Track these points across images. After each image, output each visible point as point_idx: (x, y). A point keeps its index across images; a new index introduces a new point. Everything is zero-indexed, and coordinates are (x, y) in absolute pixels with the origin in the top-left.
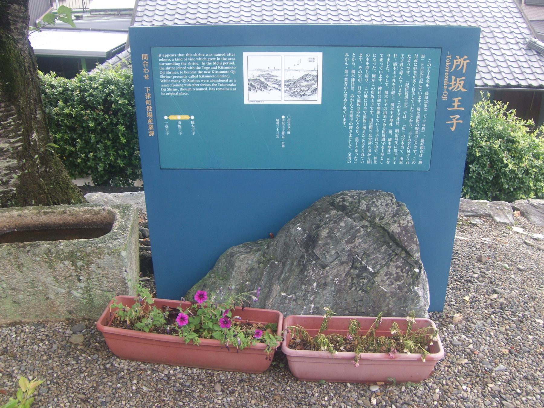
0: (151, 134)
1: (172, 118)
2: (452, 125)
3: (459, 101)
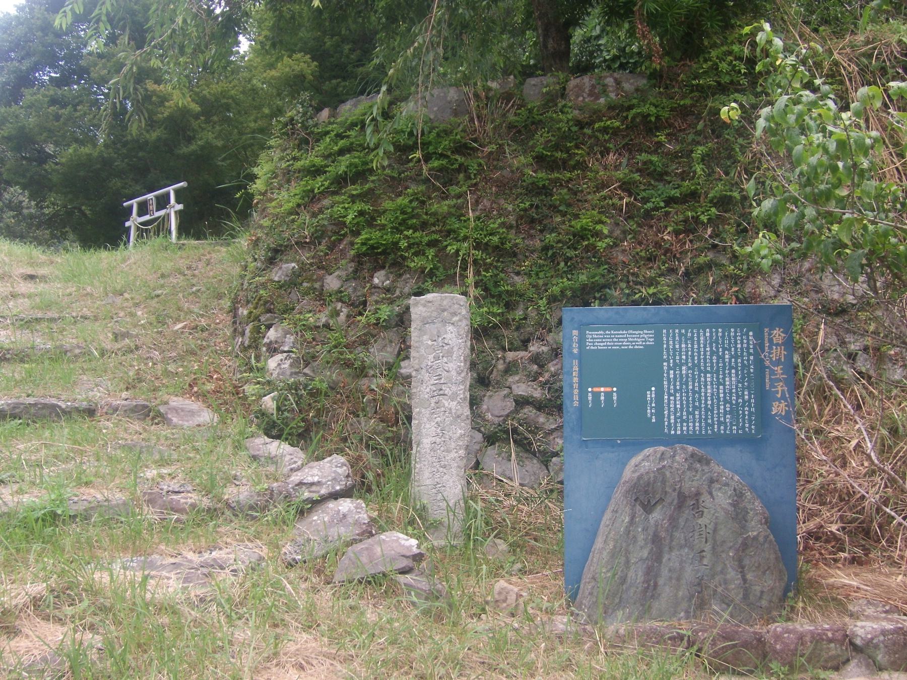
0: (576, 404)
1: (596, 389)
2: (777, 392)
3: (781, 369)
